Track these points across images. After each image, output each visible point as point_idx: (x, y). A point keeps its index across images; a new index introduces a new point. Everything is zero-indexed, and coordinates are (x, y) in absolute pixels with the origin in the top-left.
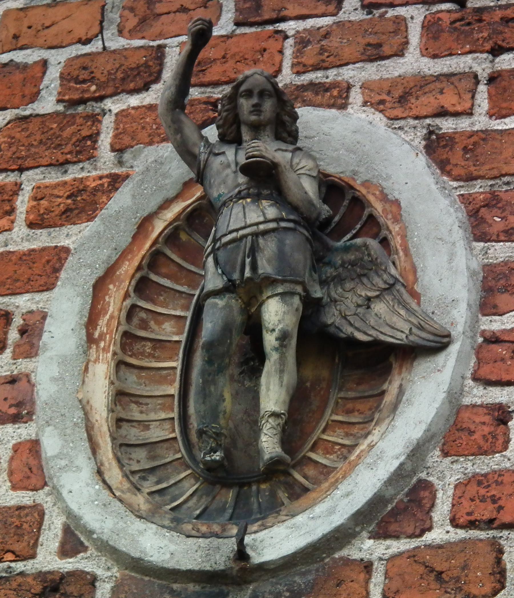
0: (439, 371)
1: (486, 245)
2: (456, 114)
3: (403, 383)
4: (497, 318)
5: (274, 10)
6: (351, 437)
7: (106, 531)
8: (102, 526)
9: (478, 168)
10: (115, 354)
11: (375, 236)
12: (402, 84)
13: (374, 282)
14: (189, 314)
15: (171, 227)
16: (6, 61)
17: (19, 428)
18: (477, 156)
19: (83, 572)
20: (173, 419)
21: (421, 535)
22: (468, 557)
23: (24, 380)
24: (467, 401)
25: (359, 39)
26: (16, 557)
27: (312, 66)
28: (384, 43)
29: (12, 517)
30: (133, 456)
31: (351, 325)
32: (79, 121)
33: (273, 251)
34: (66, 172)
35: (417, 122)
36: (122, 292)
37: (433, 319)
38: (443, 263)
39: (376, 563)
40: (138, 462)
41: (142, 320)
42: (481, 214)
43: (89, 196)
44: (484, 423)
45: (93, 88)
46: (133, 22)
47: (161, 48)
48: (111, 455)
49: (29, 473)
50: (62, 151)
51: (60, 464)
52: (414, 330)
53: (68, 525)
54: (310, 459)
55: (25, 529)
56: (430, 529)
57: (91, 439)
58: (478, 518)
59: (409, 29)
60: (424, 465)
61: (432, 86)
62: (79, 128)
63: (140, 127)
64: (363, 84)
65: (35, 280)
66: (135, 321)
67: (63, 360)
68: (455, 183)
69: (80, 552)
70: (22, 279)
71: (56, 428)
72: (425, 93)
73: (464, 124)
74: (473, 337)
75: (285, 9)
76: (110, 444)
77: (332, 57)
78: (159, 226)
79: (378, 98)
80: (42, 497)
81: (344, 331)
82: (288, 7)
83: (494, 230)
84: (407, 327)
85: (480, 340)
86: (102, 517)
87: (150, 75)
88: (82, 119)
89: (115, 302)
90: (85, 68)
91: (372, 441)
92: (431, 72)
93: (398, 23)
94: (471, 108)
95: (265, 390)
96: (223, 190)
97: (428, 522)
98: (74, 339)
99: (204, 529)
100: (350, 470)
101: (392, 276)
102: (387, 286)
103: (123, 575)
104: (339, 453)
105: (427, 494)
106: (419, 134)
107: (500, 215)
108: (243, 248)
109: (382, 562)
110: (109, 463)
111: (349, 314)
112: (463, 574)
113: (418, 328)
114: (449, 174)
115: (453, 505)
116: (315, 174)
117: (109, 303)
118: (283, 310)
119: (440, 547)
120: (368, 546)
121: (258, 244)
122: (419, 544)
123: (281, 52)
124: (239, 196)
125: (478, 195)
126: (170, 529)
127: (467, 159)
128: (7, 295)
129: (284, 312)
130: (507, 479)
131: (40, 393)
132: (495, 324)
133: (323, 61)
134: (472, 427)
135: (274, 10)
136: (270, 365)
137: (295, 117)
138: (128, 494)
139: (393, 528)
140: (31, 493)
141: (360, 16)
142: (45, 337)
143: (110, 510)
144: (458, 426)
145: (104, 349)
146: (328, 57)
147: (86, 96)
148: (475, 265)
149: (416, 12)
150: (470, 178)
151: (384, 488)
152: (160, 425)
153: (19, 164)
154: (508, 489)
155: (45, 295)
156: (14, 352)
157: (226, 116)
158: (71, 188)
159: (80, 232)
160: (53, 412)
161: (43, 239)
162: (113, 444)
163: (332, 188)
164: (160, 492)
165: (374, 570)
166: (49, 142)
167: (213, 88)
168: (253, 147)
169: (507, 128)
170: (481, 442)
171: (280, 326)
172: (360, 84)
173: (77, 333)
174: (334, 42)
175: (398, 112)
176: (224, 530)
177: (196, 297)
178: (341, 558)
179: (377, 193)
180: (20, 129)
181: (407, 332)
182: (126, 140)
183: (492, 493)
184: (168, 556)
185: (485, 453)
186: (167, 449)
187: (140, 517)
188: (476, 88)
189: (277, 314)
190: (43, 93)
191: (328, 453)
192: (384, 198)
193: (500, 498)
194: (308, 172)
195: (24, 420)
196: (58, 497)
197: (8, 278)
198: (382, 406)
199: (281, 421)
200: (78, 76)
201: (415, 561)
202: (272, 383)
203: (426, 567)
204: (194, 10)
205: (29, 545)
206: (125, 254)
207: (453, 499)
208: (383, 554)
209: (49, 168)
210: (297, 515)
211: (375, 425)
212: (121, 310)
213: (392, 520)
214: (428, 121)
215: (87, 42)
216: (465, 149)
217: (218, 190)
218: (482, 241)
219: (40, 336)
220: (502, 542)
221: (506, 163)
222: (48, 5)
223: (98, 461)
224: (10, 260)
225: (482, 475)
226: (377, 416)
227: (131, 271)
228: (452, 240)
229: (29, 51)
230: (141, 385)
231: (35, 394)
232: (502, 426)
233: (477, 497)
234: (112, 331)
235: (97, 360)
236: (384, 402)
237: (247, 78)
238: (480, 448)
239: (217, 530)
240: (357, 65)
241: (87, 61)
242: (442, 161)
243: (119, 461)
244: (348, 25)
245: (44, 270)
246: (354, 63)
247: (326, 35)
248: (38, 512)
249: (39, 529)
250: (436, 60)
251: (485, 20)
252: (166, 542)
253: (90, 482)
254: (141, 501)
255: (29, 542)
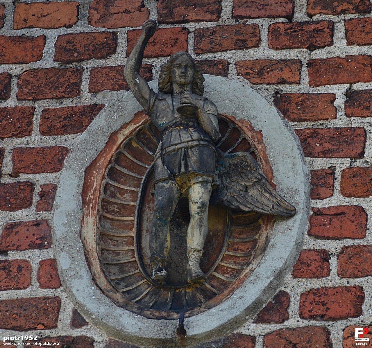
0: (290, 229)
1: (312, 159)
2: (291, 83)
3: (269, 235)
4: (320, 201)
5: (181, 16)
6: (238, 265)
7: (100, 314)
8: (98, 311)
9: (305, 115)
10: (98, 211)
11: (247, 150)
12: (259, 64)
13: (249, 177)
14: (140, 190)
15: (128, 139)
16: (21, 35)
17: (43, 252)
18: (304, 108)
19: (86, 337)
20: (133, 250)
21: (283, 322)
22: (311, 335)
23: (45, 223)
24: (305, 247)
25: (233, 36)
26: (45, 327)
27: (206, 50)
28: (247, 40)
29: (41, 303)
30: (111, 270)
31: (237, 201)
32: (69, 73)
33: (197, 157)
34: (62, 103)
35: (269, 86)
36: (101, 175)
37: (285, 200)
38: (289, 168)
39: (257, 337)
40: (114, 274)
41: (112, 192)
42: (308, 141)
43: (77, 118)
44: (315, 260)
45: (76, 55)
46: (96, 17)
47: (115, 34)
48: (99, 270)
49: (50, 278)
50: (59, 90)
51: (71, 274)
52: (275, 206)
53: (76, 310)
54: (214, 276)
55: (50, 311)
56: (288, 319)
57: (87, 260)
58: (316, 314)
59: (261, 32)
60: (283, 283)
61: (276, 66)
62: (69, 77)
63: (106, 79)
64: (236, 62)
65: (47, 165)
66: (108, 192)
67: (69, 214)
68: (292, 122)
69: (84, 325)
70: (39, 165)
71: (67, 253)
72: (273, 70)
73: (294, 89)
74: (308, 211)
75: (188, 15)
76: (98, 263)
77: (218, 46)
78: (121, 138)
79: (245, 72)
80: (58, 292)
81: (234, 204)
82: (189, 15)
83: (316, 150)
84: (270, 204)
85: (311, 213)
86: (97, 306)
87: (110, 49)
88: (70, 72)
89: (97, 180)
90: (70, 42)
91: (252, 268)
92: (275, 58)
93: (255, 28)
94: (300, 81)
95: (191, 236)
96: (165, 120)
97: (287, 314)
98: (74, 202)
99: (157, 314)
100: (241, 283)
101: (260, 174)
102: (257, 180)
103: (110, 339)
104: (231, 273)
105: (285, 299)
106: (270, 93)
107: (319, 142)
108: (179, 155)
109: (261, 337)
110: (99, 275)
111: (236, 195)
112: (308, 345)
113: (277, 205)
114: (288, 117)
115: (300, 306)
116: (216, 115)
117: (94, 181)
118: (202, 191)
119: (294, 329)
120: (253, 327)
121: (188, 153)
122: (282, 327)
123: (187, 41)
124: (176, 125)
125: (305, 130)
126: (138, 314)
127: (299, 110)
128: (31, 173)
129: (203, 193)
130: (330, 292)
131: (56, 232)
132: (320, 204)
133: (213, 48)
134: (309, 262)
135: (181, 16)
136: (193, 222)
137: (203, 80)
138: (111, 293)
139: (266, 317)
140: (52, 290)
141: (232, 22)
142: (57, 200)
143: (102, 302)
144: (301, 261)
145: (92, 208)
146: (215, 46)
147: (72, 59)
148: (307, 171)
149: (264, 22)
150: (301, 120)
151: (262, 295)
152: (126, 253)
153: (33, 96)
154: (331, 298)
155: (55, 174)
156: (37, 207)
157: (165, 78)
158: (66, 113)
159: (73, 139)
160: (65, 243)
161: (50, 141)
162: (100, 263)
163: (224, 122)
164: (128, 292)
165: (257, 341)
166: (51, 85)
167: (148, 59)
168: (185, 97)
169: (320, 93)
170: (314, 270)
171: (201, 200)
172: (234, 62)
173: (76, 198)
174: (217, 38)
175: (257, 80)
176: (169, 315)
177: (143, 181)
178: (238, 334)
179: (248, 126)
180: (32, 76)
181: (271, 207)
182: (99, 87)
183: (322, 300)
184: (138, 329)
185: (317, 277)
186: (130, 267)
187: (120, 306)
188: (301, 69)
189: (198, 193)
190: (45, 55)
191: (225, 273)
192: (252, 129)
193: (327, 303)
194: (212, 113)
195: (46, 247)
196: (71, 294)
197: (31, 164)
198: (256, 248)
199: (200, 254)
200: (66, 47)
201: (280, 337)
202: (195, 231)
203: (287, 340)
204: (133, 12)
205: (52, 320)
206: (101, 154)
207: (300, 302)
208: (262, 332)
209: (52, 100)
210: (212, 307)
211: (253, 259)
212: (100, 186)
213: (266, 313)
214: (275, 86)
215: (70, 26)
216: (297, 103)
217: (162, 120)
218: (309, 157)
219: (53, 200)
220: (329, 328)
221: (321, 113)
222: (44, 3)
223: (92, 273)
224: (32, 153)
225: (316, 290)
226: (253, 253)
227: (106, 164)
228: (293, 155)
229: (34, 29)
230: (113, 229)
231: (52, 233)
232: (326, 262)
233: (313, 302)
234: (96, 198)
235: (88, 214)
236: (257, 246)
237: (178, 57)
238: (314, 274)
239: (164, 315)
240: (232, 51)
241: (70, 38)
242: (284, 110)
243: (104, 272)
244: (225, 27)
245: (54, 160)
246: (231, 50)
247: (213, 33)
248: (57, 301)
249: (58, 312)
250: (277, 51)
251: (305, 30)
252: (136, 321)
253: (89, 285)
254: (118, 296)
255: (53, 319)
